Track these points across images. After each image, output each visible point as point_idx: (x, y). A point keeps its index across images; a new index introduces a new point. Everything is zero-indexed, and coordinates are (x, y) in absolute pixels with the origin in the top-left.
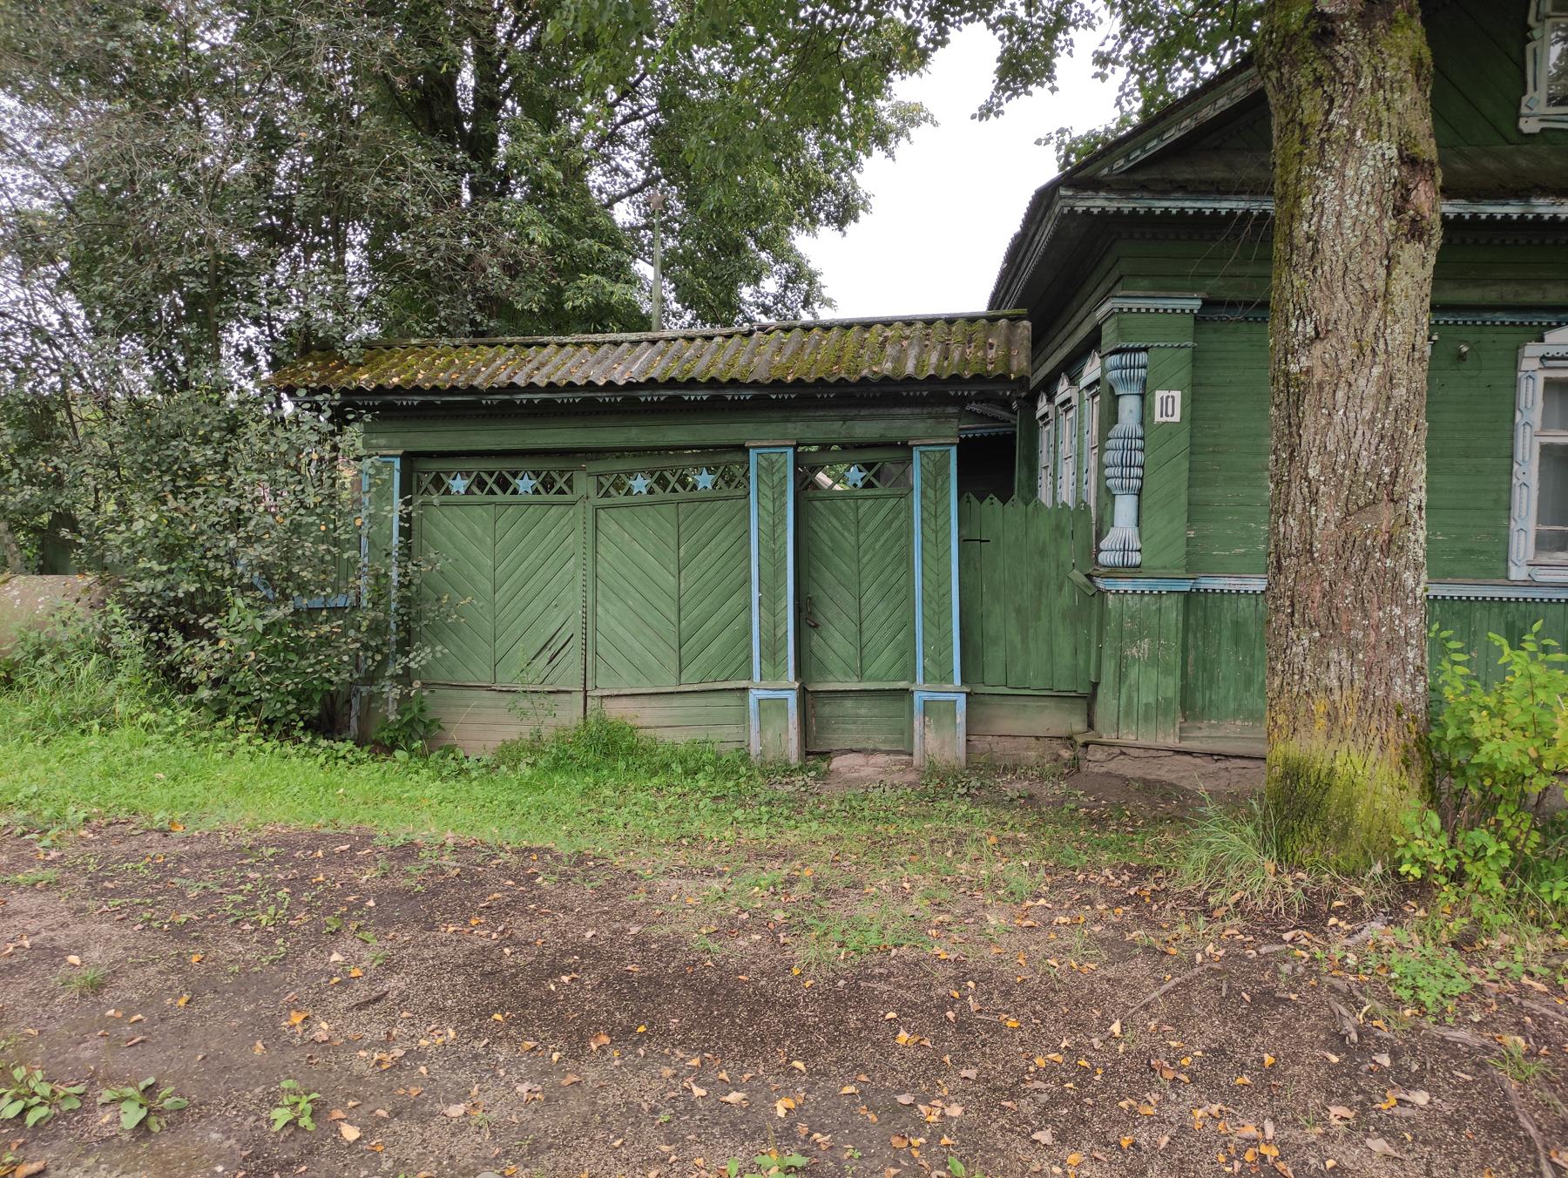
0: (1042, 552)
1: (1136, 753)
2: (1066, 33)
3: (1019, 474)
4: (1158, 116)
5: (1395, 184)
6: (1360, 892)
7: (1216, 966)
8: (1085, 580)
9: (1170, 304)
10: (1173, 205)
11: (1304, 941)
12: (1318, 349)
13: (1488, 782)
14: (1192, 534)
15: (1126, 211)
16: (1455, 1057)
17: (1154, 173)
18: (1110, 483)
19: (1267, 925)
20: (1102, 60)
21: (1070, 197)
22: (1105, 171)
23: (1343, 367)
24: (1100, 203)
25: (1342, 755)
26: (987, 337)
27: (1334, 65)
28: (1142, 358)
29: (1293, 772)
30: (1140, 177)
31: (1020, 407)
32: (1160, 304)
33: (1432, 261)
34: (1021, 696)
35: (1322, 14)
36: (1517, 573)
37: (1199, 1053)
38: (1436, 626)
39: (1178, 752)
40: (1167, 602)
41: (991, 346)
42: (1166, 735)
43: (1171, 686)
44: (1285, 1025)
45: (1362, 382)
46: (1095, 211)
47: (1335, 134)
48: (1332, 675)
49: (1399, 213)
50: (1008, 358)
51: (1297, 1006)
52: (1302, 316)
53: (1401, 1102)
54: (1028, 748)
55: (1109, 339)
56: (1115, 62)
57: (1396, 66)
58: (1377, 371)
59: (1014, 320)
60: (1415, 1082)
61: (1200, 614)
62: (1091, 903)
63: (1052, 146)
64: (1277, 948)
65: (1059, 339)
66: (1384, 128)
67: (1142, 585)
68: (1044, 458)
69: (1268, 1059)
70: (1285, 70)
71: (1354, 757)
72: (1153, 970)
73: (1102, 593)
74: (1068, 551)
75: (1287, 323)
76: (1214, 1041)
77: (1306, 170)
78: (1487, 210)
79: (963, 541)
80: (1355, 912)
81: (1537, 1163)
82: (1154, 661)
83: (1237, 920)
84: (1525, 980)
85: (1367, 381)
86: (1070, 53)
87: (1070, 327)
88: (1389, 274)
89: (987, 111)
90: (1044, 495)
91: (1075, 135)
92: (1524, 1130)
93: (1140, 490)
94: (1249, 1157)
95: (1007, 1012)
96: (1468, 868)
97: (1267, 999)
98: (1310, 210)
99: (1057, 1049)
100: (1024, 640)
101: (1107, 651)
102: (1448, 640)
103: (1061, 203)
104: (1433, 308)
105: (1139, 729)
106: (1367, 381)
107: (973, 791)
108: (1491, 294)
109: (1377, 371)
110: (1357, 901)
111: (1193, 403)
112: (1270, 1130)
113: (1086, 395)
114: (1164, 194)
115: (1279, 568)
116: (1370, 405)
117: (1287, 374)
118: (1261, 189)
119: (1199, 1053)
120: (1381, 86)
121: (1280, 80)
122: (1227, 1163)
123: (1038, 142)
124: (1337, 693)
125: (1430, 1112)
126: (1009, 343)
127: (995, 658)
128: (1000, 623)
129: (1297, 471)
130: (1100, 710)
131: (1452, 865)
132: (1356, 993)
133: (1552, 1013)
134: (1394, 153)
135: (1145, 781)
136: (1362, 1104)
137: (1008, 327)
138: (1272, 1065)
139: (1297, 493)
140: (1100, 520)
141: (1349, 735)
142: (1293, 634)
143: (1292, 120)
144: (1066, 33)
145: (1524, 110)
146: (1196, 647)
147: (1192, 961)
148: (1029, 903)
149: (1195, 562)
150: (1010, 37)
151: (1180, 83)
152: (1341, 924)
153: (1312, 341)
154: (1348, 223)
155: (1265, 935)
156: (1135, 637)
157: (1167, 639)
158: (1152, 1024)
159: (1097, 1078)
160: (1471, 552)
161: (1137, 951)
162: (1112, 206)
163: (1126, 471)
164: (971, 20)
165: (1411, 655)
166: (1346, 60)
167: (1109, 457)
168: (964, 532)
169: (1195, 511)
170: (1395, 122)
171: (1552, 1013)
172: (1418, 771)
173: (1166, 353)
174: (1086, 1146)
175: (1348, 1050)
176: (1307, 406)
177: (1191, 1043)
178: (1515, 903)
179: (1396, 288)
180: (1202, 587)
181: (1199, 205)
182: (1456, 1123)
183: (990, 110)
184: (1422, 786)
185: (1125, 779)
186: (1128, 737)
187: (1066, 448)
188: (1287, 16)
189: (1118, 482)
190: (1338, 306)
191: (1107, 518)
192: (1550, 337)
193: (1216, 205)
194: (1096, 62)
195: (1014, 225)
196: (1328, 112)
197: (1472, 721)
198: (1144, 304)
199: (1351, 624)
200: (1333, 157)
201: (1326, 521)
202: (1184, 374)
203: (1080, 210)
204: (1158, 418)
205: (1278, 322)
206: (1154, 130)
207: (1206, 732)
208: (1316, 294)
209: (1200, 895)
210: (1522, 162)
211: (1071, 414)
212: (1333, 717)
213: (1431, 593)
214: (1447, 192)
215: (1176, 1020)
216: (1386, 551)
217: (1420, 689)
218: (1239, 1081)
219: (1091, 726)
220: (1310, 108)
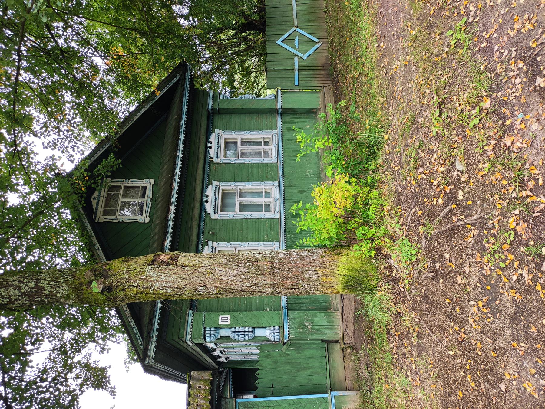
0: (276, 362)
1: (345, 326)
2: (91, 364)
3: (246, 366)
4: (126, 328)
5: (160, 266)
6: (383, 267)
7: (419, 315)
8: (285, 346)
9: (190, 321)
10: (157, 321)
11: (403, 285)
12: (209, 285)
13: (342, 232)
14: (268, 309)
15: (156, 339)
16: (431, 245)
17: (145, 329)
18: (250, 338)
19: (400, 296)
20: (103, 350)
21: (149, 359)
22: (142, 347)
23: (215, 278)
24: (152, 348)
25: (339, 272)
26: (196, 389)
27: (119, 286)
28: (207, 329)
29: (347, 286)
30: (145, 335)
31: (222, 368)
32: (190, 324)
33: (184, 253)
34: (330, 369)
35: (103, 290)
36: (277, 216)
37: (452, 324)
38: (296, 247)
39: (343, 311)
40: (291, 317)
41: (199, 387)
42: (337, 315)
43: (320, 314)
44: (434, 294)
45: (220, 272)
46: (155, 349)
47: (141, 284)
48: (313, 276)
49: (168, 264)
50: (205, 381)
51: (426, 290)
52: (198, 291)
53: (450, 261)
54: (349, 365)
55: (200, 341)
56: (104, 345)
57: (123, 267)
58: (217, 268)
59: (190, 378)
60: (442, 257)
61: (295, 305)
62: (405, 354)
63: (129, 365)
64: (407, 294)
65: (199, 356)
66: (142, 270)
67: (286, 325)
68: (241, 358)
69: (447, 301)
70: (118, 299)
71: (339, 269)
72: (425, 336)
73: (290, 339)
74: (275, 352)
75: (200, 295)
76: (446, 318)
77: (151, 292)
78: (170, 230)
79: (273, 395)
80: (390, 268)
81: (458, 226)
82: (312, 321)
83: (401, 305)
84: (401, 223)
85: (220, 271)
86: (98, 362)
87: (195, 353)
88: (187, 266)
89: (113, 393)
90: (255, 357)
91: (127, 357)
92: (449, 228)
93: (253, 327)
94: (485, 311)
95: (456, 395)
96: (369, 237)
97: (426, 298)
98: (164, 290)
99: (466, 377)
100: (309, 368)
101: (310, 337)
102: (299, 243)
103: (150, 363)
104: (197, 253)
105: (336, 325)
106: (220, 271)
107: (368, 388)
108: (195, 227)
109: (217, 268)
110: (385, 267)
111: (223, 311)
112: (472, 303)
113: (219, 346)
114: (152, 326)
115: (280, 293)
116: (227, 270)
117: (217, 294)
118: (153, 304)
119: (452, 324)
120: (129, 271)
121: (120, 301)
122: (490, 318)
123: (127, 371)
124: (319, 275)
125: (452, 253)
126: (199, 380)
127: (317, 380)
128: (303, 378)
129: (248, 289)
130: (331, 339)
131: (369, 242)
132: (417, 271)
133: (409, 218)
134: (150, 267)
135: (355, 322)
136: (454, 273)
137: (193, 380)
138: (450, 300)
139: (255, 289)
140: (264, 341)
141: (333, 271)
142: (301, 288)
143: (135, 297)
144: (91, 364)
145: (143, 222)
146: (306, 306)
147: (419, 323)
148: (410, 379)
149: (278, 308)
150: (88, 385)
151: (116, 321)
152: (394, 272)
153: (206, 287)
154: (170, 279)
155: (404, 297)
156: (305, 327)
157: (304, 316)
158: (446, 339)
159: (472, 362)
160: (271, 228)
161: (420, 342)
162: (154, 344)
163: (246, 333)
164: (78, 402)
165: (305, 254)
166: (118, 282)
167: (241, 339)
168: (269, 394)
169: (260, 309)
170: (140, 267)
171: (409, 218)
172: (341, 251)
173: (207, 321)
174: (500, 370)
175: (437, 276)
176: (225, 287)
177: (449, 326)
178: (378, 225)
179: (192, 264)
180: (285, 305)
181: (158, 314)
182: (453, 247)
183: (113, 391)
184: (345, 249)
185: (355, 329)
186: (340, 328)
187: (237, 351)
188: (100, 300)
189: (250, 335)
190: (196, 280)
191: (263, 338)
192: (208, 211)
193: (159, 308)
194: (103, 353)
195: (157, 378)
196: (134, 287)
197: (324, 238)
198: (189, 330)
199: (296, 272)
200: (148, 285)
201: (264, 280)
202: (214, 315)
203: (154, 355)
204: (228, 323)
205: (200, 298)
206: (130, 330)
207: (335, 303)
208: (191, 287)
209: (394, 316)
210: (158, 221)
211: (226, 350)
212: (327, 276)
213: (284, 248)
214: (162, 250)
215: (442, 331)
216: (273, 263)
217: (315, 251)
218: (458, 311)
219: (337, 342)
220: (131, 292)
